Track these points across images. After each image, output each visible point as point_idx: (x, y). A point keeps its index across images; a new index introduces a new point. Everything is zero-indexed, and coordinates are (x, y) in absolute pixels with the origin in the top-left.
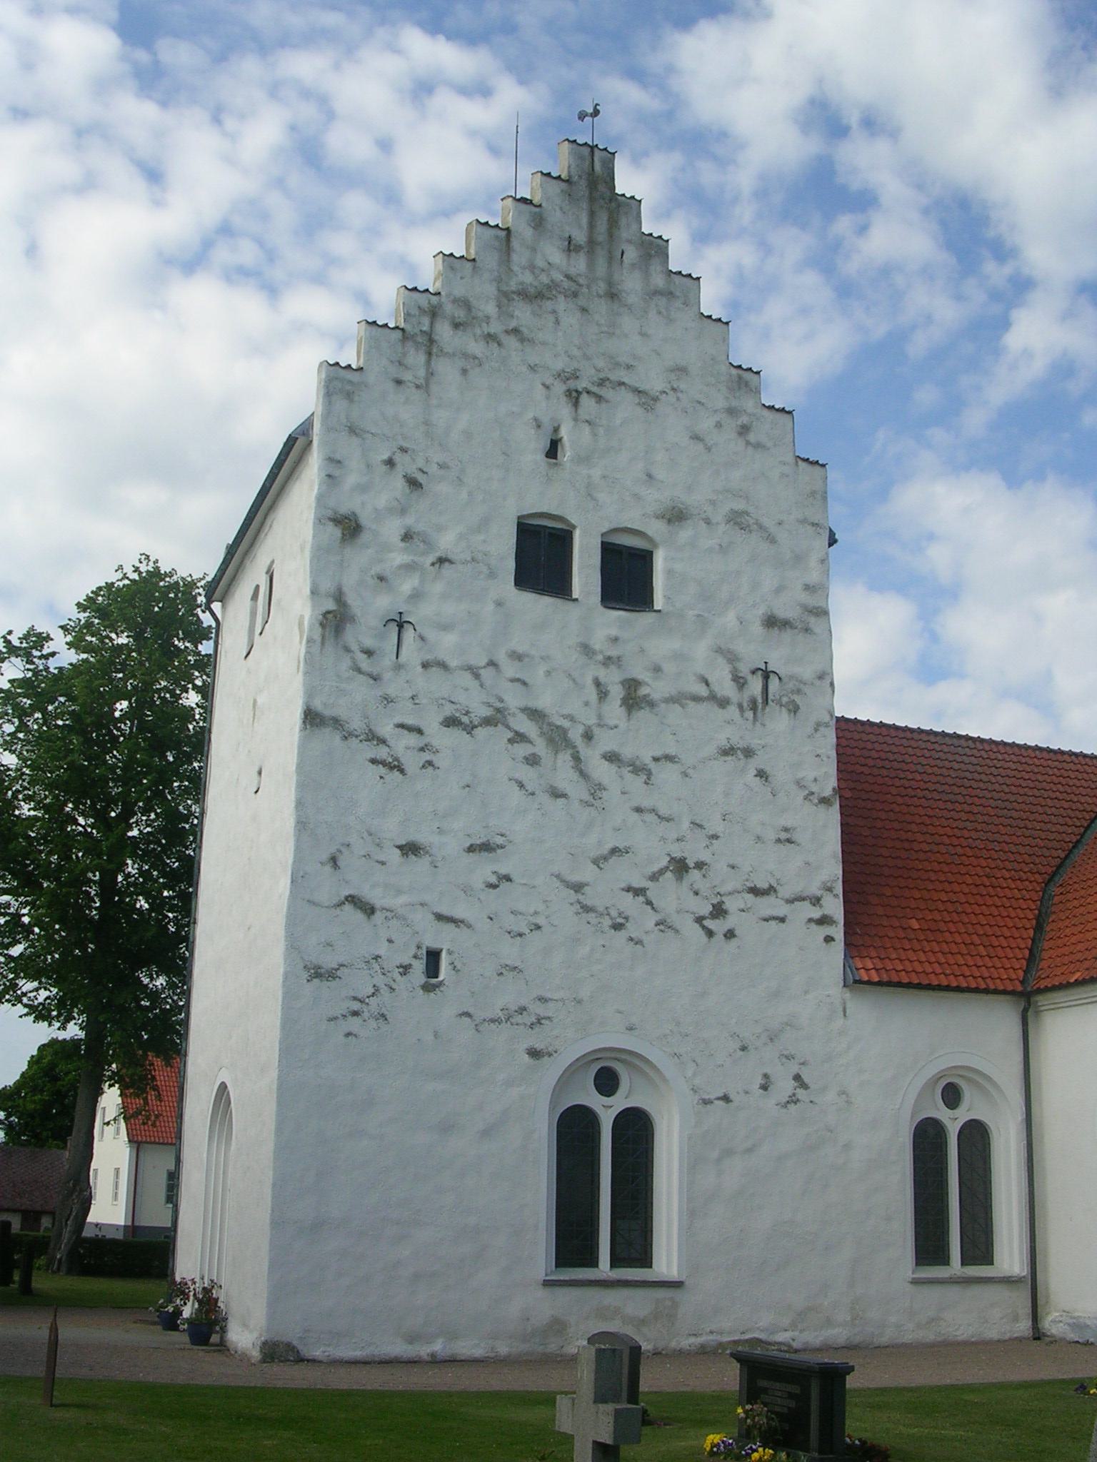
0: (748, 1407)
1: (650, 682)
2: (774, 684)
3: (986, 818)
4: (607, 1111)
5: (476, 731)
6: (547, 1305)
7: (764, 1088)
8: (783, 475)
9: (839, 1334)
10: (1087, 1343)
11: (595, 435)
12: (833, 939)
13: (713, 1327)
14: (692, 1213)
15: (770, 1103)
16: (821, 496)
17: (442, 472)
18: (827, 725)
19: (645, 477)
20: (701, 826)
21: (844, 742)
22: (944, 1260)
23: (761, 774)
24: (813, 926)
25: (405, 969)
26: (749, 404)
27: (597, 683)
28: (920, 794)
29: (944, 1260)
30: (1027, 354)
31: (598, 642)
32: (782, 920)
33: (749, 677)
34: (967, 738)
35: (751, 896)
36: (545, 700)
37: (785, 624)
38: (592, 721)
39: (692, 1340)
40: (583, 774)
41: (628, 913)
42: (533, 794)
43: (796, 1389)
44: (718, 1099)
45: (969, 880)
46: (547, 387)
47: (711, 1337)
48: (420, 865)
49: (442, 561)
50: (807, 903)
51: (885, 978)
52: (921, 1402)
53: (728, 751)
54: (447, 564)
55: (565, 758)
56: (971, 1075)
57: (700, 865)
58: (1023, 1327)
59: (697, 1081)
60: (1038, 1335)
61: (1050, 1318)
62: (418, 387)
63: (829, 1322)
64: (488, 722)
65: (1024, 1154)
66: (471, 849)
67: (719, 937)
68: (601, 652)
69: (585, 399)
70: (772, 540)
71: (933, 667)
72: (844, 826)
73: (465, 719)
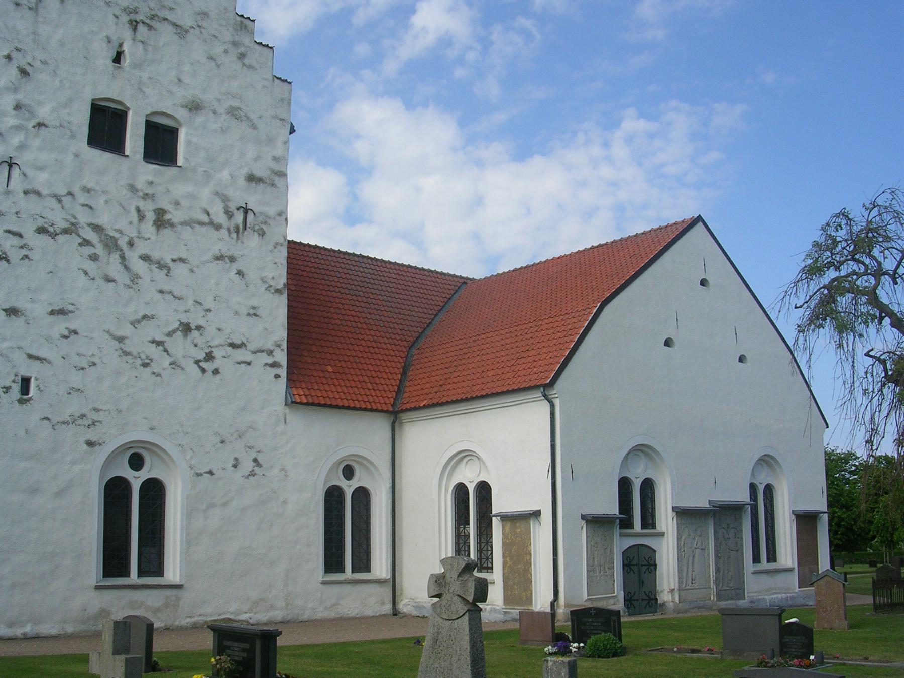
0: (218, 658)
1: (171, 210)
2: (250, 217)
3: (376, 307)
4: (136, 479)
5: (57, 237)
6: (97, 601)
7: (235, 466)
8: (264, 87)
9: (278, 615)
10: (424, 617)
11: (145, 50)
12: (280, 376)
13: (202, 612)
14: (188, 543)
15: (238, 475)
16: (287, 102)
17: (43, 66)
18: (282, 245)
19: (176, 80)
20: (200, 304)
21: (292, 256)
22: (341, 570)
23: (240, 273)
24: (268, 368)
25: (7, 389)
26: (246, 40)
27: (138, 210)
28: (337, 290)
29: (341, 570)
30: (425, 30)
31: (140, 184)
32: (249, 363)
33: (235, 212)
34: (368, 258)
35: (230, 348)
36: (104, 220)
37: (259, 180)
38: (134, 234)
39: (188, 620)
40: (126, 268)
41: (152, 356)
42: (93, 279)
43: (246, 646)
44: (207, 473)
45: (364, 343)
46: (117, 17)
47: (200, 618)
48: (18, 322)
49: (40, 125)
50: (264, 354)
51: (311, 400)
52: (324, 653)
53: (219, 258)
54: (43, 127)
55: (115, 257)
56: (360, 460)
57: (199, 328)
58: (387, 608)
59: (193, 462)
60: (395, 612)
61: (403, 603)
62: (30, 9)
63: (272, 607)
64: (65, 231)
65: (390, 507)
66: (52, 313)
67: (209, 373)
68: (142, 190)
69: (141, 27)
70: (254, 127)
71: (353, 216)
72: (289, 307)
73: (51, 229)
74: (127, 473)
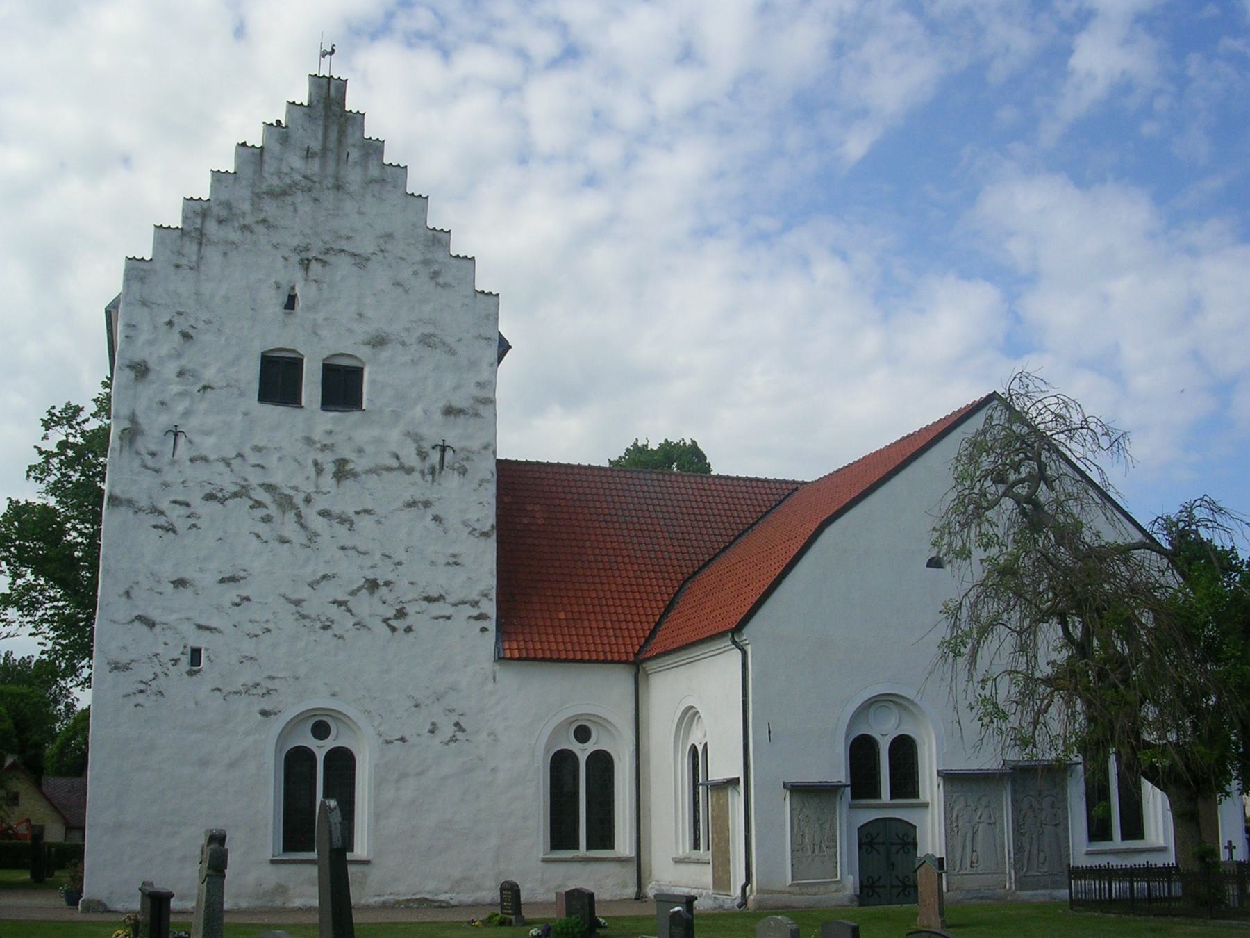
4: (582, 752)
37: (460, 412)
40: (303, 526)
70: (452, 352)
74: (575, 747)
